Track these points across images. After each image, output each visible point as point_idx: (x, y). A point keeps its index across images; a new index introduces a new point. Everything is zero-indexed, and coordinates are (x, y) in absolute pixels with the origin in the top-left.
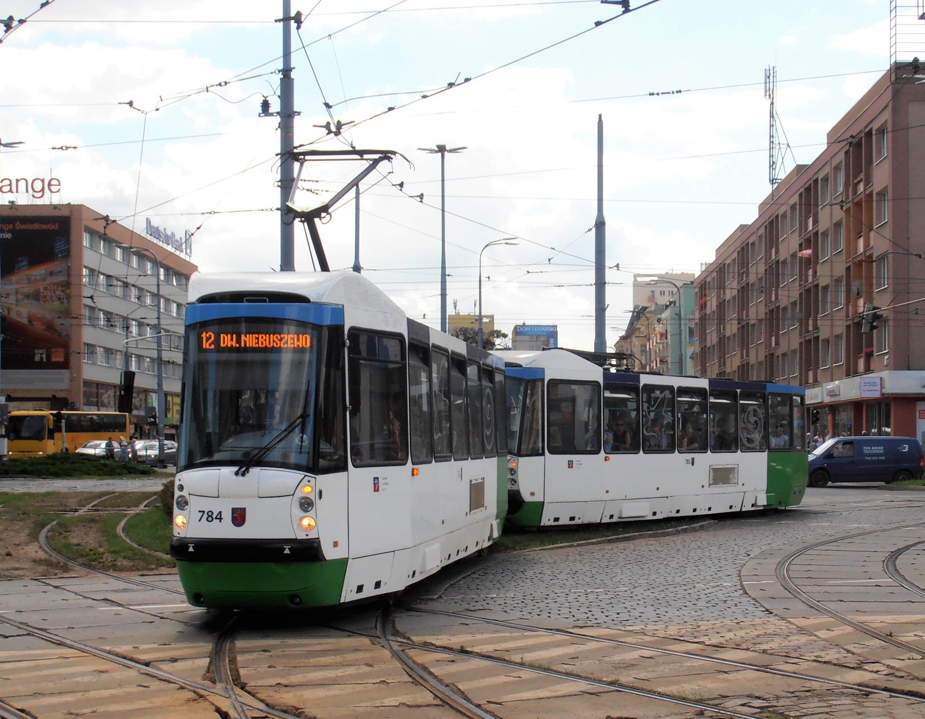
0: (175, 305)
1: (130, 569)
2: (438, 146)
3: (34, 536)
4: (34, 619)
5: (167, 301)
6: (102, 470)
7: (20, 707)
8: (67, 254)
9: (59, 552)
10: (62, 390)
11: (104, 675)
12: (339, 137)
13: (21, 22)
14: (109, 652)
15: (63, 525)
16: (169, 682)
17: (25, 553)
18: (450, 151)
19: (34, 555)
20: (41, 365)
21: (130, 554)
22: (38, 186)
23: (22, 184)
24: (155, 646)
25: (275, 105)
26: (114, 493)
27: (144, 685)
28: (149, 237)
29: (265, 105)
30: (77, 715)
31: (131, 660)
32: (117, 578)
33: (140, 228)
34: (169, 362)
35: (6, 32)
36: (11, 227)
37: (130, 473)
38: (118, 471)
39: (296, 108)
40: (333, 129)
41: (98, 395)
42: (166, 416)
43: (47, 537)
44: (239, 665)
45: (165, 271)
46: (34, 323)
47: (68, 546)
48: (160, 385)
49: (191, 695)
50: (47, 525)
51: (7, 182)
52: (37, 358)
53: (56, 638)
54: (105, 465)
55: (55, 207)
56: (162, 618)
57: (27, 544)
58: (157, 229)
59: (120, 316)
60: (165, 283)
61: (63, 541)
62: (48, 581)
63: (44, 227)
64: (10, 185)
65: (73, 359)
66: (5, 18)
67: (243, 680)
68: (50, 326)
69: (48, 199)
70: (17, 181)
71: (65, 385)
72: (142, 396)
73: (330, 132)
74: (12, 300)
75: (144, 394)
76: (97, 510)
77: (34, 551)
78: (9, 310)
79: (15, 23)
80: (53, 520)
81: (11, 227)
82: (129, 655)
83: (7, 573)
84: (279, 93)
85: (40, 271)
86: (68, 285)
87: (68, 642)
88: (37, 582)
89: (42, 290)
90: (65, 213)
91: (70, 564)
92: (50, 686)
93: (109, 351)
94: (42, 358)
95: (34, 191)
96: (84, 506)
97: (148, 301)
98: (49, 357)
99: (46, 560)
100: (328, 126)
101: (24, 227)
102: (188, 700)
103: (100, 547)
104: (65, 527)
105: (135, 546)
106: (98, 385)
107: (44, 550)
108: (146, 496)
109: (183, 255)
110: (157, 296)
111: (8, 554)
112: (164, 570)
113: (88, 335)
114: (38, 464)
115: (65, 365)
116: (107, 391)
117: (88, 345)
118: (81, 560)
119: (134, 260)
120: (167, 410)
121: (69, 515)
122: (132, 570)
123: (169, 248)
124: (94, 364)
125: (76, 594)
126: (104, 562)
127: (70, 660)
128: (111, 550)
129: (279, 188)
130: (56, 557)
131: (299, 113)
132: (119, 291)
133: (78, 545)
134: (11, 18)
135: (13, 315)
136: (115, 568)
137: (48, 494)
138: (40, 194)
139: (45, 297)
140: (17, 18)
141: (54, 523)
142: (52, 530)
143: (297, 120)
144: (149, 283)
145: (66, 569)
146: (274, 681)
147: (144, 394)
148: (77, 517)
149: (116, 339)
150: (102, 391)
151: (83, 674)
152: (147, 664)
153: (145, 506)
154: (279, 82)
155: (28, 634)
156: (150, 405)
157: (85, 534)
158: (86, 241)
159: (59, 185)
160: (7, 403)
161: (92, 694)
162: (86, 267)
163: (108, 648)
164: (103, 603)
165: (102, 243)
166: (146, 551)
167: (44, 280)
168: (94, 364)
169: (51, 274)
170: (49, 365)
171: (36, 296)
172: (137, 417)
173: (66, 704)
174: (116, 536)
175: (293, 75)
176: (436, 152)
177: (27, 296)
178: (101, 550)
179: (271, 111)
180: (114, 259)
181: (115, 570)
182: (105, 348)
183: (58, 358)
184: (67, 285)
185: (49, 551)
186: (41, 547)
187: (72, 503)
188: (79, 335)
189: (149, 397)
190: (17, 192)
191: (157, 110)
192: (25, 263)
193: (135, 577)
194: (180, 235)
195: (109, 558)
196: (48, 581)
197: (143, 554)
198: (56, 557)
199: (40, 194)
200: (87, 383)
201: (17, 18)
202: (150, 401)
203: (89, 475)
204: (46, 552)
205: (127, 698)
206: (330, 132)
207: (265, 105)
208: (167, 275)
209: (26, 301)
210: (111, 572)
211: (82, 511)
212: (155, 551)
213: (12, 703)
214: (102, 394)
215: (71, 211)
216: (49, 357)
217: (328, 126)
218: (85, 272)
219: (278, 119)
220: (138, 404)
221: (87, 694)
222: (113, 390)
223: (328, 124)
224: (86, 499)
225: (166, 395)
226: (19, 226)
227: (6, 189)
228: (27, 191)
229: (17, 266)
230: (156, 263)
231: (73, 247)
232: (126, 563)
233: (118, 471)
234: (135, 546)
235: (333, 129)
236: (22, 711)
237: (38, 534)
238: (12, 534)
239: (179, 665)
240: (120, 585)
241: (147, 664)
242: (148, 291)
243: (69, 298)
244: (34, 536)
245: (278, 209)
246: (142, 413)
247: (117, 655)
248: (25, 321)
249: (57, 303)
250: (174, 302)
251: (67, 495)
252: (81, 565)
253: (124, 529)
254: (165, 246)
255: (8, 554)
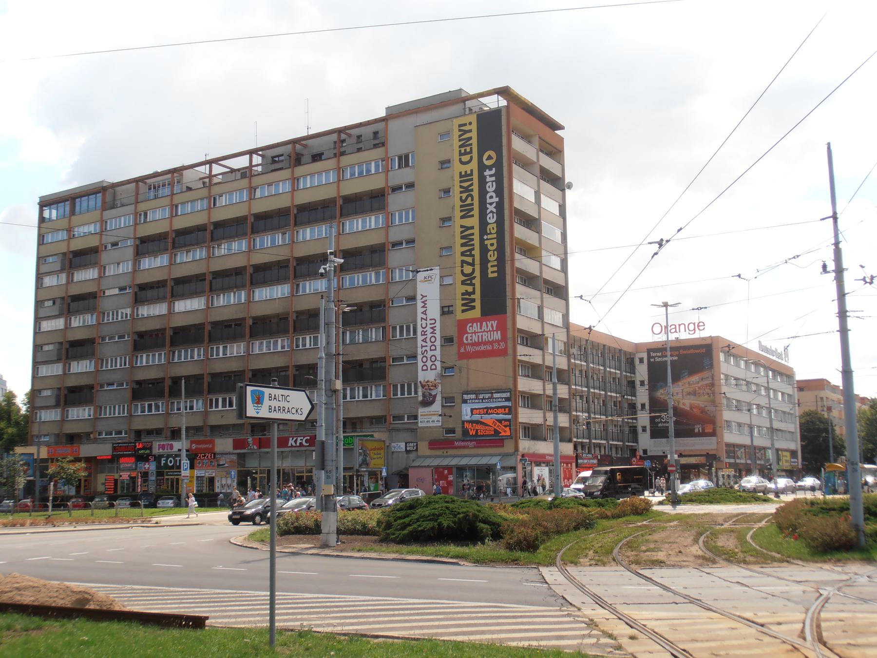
0: (780, 393)
1: (755, 563)
2: (663, 303)
3: (696, 541)
4: (693, 593)
5: (775, 391)
6: (738, 499)
7: (682, 648)
8: (711, 366)
9: (710, 551)
10: (712, 450)
11: (734, 631)
12: (872, 285)
13: (668, 241)
14: (739, 616)
15: (714, 534)
16: (776, 638)
17: (690, 551)
18: (671, 306)
19: (695, 553)
20: (699, 435)
21: (754, 553)
22: (692, 327)
23: (682, 327)
24: (768, 614)
25: (831, 266)
26: (746, 513)
27: (760, 638)
28: (761, 352)
29: (824, 267)
30: (716, 655)
31: (753, 622)
32: (746, 569)
33: (754, 347)
34: (777, 430)
35: (659, 248)
36: (677, 353)
37: (756, 500)
38: (749, 499)
39: (844, 266)
40: (868, 280)
41: (734, 452)
42: (779, 464)
43: (703, 541)
44: (823, 629)
45: (772, 374)
46: (694, 409)
47: (716, 547)
48: (772, 445)
49: (790, 647)
50: (704, 534)
51: (674, 327)
52: (696, 430)
53: (706, 605)
54: (740, 496)
55: (703, 339)
56: (773, 595)
57: (691, 546)
58: (766, 347)
59: (746, 402)
60: (773, 381)
61: (713, 544)
62: (703, 570)
63: (697, 351)
64: (675, 328)
65: (718, 429)
66: (659, 240)
67: (825, 639)
68: (703, 411)
69: (698, 335)
70: (679, 325)
71: (714, 446)
72: (762, 452)
73: (866, 282)
74: (680, 396)
75: (763, 451)
76: (735, 525)
77: (696, 550)
78: (678, 402)
79: (664, 242)
80: (708, 531)
81: (677, 353)
82: (751, 619)
83: (679, 564)
84: (833, 258)
85: (695, 378)
86: (712, 387)
87: (714, 609)
88: (696, 570)
89: (697, 390)
90: (708, 342)
91: (717, 559)
92: (700, 636)
93: (740, 425)
94: (699, 430)
95: (689, 330)
96: (727, 522)
97: (763, 393)
98: (703, 429)
99: (702, 556)
100: (864, 279)
101: (685, 352)
102: (788, 651)
103: (736, 548)
104: (715, 535)
105: (758, 548)
106: (734, 446)
107: (701, 550)
108: (765, 516)
109: (783, 362)
110: (767, 389)
111: (680, 552)
112: (775, 564)
113: (727, 415)
114: (699, 496)
115: (713, 434)
116: (740, 450)
117: (726, 421)
118: (723, 557)
119: (753, 367)
120: (778, 460)
121: (718, 527)
122: (755, 564)
123: (774, 358)
124: (731, 432)
125: (720, 578)
126: (738, 558)
127: (715, 620)
128: (744, 550)
129: (838, 318)
130: (709, 554)
131: (847, 269)
132: (744, 388)
133: (723, 547)
134: (662, 240)
135: (681, 406)
136: (745, 562)
137: (705, 514)
138: (693, 332)
139: (699, 393)
140: (665, 239)
141: (708, 533)
142: (707, 537)
143: (845, 274)
144: (762, 381)
145: (714, 562)
146: (845, 642)
147: (763, 451)
148: (722, 529)
149: (743, 417)
150: (736, 449)
151: (721, 629)
152: (762, 625)
153: (766, 522)
154: (833, 251)
155: (690, 603)
156: (767, 457)
157: (727, 540)
158: (722, 357)
159: (704, 325)
160: (679, 458)
161: (727, 643)
162: (723, 374)
163: (738, 614)
164: (736, 585)
165: (732, 358)
166: (765, 551)
167: (698, 383)
168: (731, 432)
169: (702, 379)
170: (703, 434)
171: (694, 393)
172: (760, 465)
173: (709, 648)
174: (746, 542)
175: (841, 246)
176: (663, 306)
177: (689, 394)
178: (737, 550)
179: (828, 269)
180: (740, 367)
181: (744, 563)
182: (737, 423)
183: (709, 430)
184: (712, 385)
185: (704, 550)
186: (700, 548)
187: (720, 520)
188: (721, 415)
189: (767, 452)
190: (680, 332)
191: (756, 278)
192: (686, 374)
193: (756, 568)
194: (780, 350)
195: (741, 556)
196: (703, 570)
197: (763, 554)
198: (709, 554)
199: (693, 332)
200: (727, 445)
201: (665, 239)
202: (767, 454)
203: (731, 502)
204: (703, 551)
205: (748, 647)
206: (866, 282)
207: (824, 267)
208: (774, 377)
209: (688, 396)
210: (742, 565)
211: (726, 525)
212: (771, 552)
213: (678, 645)
214: (737, 451)
215: (712, 340)
216: (703, 429)
217: (864, 279)
218: (722, 376)
219: (833, 274)
220: (760, 457)
221: (723, 642)
222: (744, 449)
223: (865, 277)
224: (728, 517)
225: (777, 450)
226: (682, 352)
227: (673, 331)
228: (685, 331)
229: (681, 376)
230: (767, 368)
231: (715, 363)
232: (752, 559)
233: (749, 499)
234: (758, 548)
235: (868, 280)
236: (684, 650)
237: (698, 539)
238: (683, 539)
239: (783, 627)
240: (748, 573)
241: (762, 625)
242: (762, 386)
243: (713, 393)
244: (696, 541)
245: (838, 331)
246: (762, 462)
247: (744, 618)
248: (687, 408)
249: (706, 397)
250: (779, 391)
251: (718, 515)
252: (724, 560)
253: (751, 537)
254: (771, 357)
255: (680, 552)
